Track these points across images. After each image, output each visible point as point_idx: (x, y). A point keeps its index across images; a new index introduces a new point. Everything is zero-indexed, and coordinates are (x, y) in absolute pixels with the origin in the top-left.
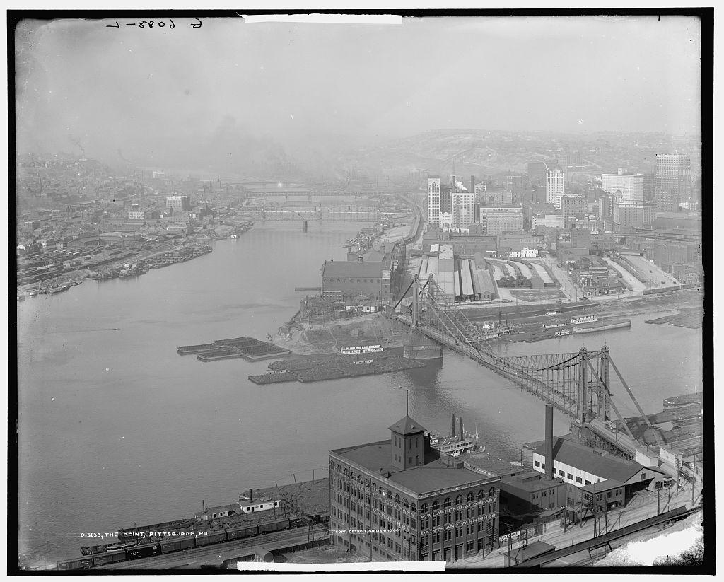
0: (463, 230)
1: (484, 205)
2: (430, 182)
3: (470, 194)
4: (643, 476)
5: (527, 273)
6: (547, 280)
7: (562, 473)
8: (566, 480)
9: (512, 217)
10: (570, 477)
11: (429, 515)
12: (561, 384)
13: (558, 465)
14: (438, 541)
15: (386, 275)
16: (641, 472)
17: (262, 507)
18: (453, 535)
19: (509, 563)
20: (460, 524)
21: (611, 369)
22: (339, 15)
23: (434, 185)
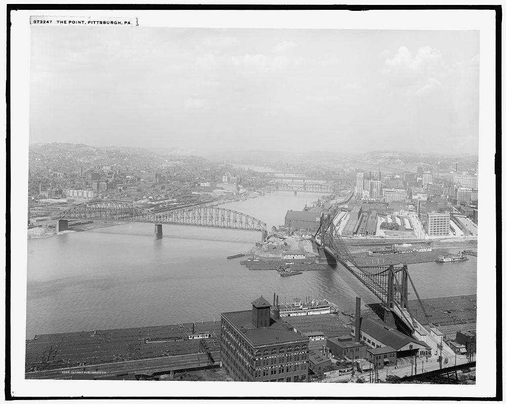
0: (372, 200)
1: (385, 187)
2: (358, 174)
3: (379, 182)
4: (411, 346)
5: (398, 221)
6: (408, 226)
7: (365, 339)
8: (366, 342)
9: (399, 194)
10: (369, 341)
11: (261, 359)
12: (384, 285)
13: (363, 334)
14: (275, 374)
15: (318, 219)
16: (409, 344)
17: (198, 337)
18: (277, 372)
19: (441, 366)
20: (282, 366)
21: (408, 279)
22: (494, 152)
23: (360, 176)
